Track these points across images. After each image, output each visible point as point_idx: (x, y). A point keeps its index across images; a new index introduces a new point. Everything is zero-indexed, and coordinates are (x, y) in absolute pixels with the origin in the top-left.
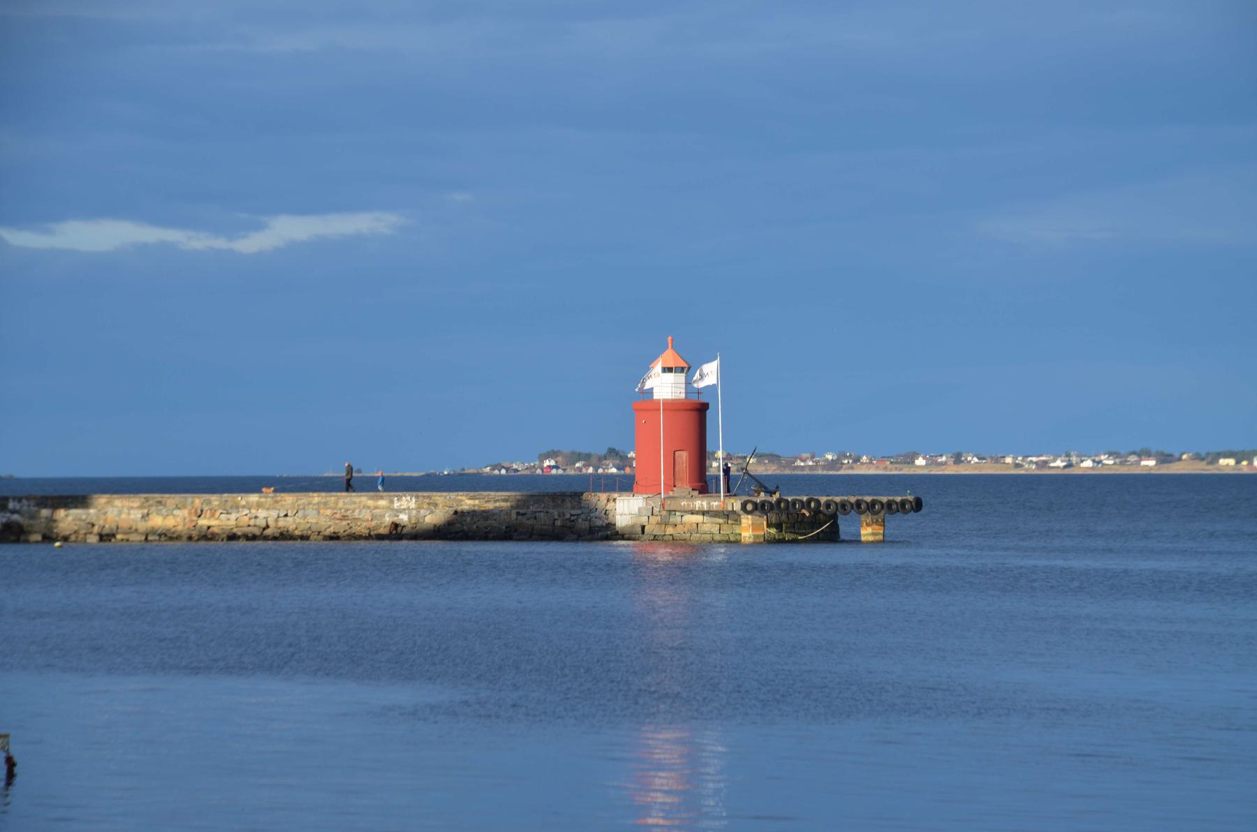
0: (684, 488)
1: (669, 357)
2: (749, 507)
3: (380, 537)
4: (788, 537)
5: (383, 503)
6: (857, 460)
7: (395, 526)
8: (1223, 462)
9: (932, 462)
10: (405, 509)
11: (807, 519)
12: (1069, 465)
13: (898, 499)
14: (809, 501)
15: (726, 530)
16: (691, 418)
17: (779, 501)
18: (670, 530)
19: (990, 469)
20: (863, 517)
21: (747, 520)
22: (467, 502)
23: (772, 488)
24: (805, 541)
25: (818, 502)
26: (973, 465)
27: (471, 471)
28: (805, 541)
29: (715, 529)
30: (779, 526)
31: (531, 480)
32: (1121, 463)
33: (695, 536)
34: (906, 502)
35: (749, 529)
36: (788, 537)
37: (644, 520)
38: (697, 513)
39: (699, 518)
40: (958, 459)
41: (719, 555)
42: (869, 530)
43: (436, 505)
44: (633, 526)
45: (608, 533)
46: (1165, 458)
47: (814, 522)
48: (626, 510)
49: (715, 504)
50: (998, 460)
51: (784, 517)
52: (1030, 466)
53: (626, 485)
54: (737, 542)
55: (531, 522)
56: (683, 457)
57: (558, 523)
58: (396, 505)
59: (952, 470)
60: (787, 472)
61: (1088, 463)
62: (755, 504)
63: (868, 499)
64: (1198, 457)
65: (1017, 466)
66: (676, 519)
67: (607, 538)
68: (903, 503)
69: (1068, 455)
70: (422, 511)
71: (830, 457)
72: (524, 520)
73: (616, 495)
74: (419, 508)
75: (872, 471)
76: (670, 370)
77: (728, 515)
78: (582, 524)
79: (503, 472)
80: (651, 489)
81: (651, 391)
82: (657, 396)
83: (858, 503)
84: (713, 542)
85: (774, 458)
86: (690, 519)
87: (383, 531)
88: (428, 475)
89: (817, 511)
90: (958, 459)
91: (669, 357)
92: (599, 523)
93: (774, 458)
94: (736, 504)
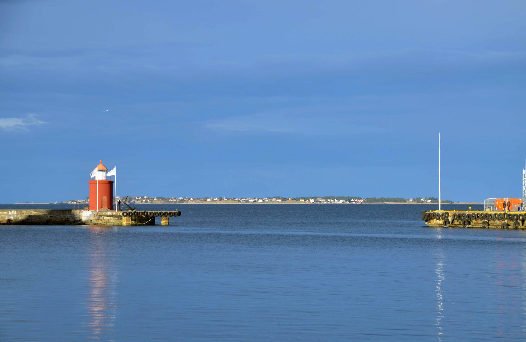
0: (105, 208)
1: (101, 166)
2: (125, 214)
3: (4, 224)
4: (138, 224)
5: (5, 213)
6: (189, 199)
7: (9, 220)
8: (301, 200)
9: (213, 200)
10: (13, 215)
11: (145, 218)
12: (255, 201)
13: (173, 212)
14: (144, 212)
15: (118, 222)
16: (108, 186)
17: (135, 212)
18: (100, 222)
19: (230, 202)
20: (162, 217)
21: (124, 218)
22: (33, 213)
23: (133, 208)
24: (144, 225)
25: (147, 213)
26: (225, 201)
27: (65, 202)
28: (144, 225)
29: (115, 221)
30: (135, 220)
31: (50, 205)
32: (271, 201)
33: (108, 224)
34: (176, 213)
35: (125, 221)
36: (138, 224)
37: (91, 218)
38: (109, 216)
39: (109, 218)
40: (221, 199)
41: (116, 229)
42: (164, 222)
43: (23, 214)
44: (88, 220)
45: (81, 223)
46: (284, 199)
47: (147, 219)
48: (85, 215)
49: (114, 213)
50: (233, 199)
51: (137, 217)
52: (243, 202)
53: (421, 198)
54: (121, 225)
55: (54, 219)
56: (105, 198)
57: (64, 219)
58: (10, 213)
59: (219, 203)
60: (167, 203)
61: (260, 201)
62: (127, 214)
63: (164, 212)
64: (294, 199)
65: (239, 201)
66: (102, 218)
67: (79, 224)
68: (175, 213)
69: (255, 198)
70: (18, 216)
71: (180, 198)
72: (52, 218)
73: (82, 210)
74: (17, 214)
75: (194, 203)
76: (101, 170)
77: (119, 217)
78: (71, 220)
79: (75, 203)
80: (94, 208)
81: (94, 177)
82: (97, 179)
83: (160, 213)
84: (114, 225)
85: (163, 199)
86: (106, 218)
87: (4, 222)
88: (50, 204)
89: (147, 216)
90: (221, 199)
91: (101, 166)
92: (77, 219)
93: (163, 199)
94: (121, 214)
